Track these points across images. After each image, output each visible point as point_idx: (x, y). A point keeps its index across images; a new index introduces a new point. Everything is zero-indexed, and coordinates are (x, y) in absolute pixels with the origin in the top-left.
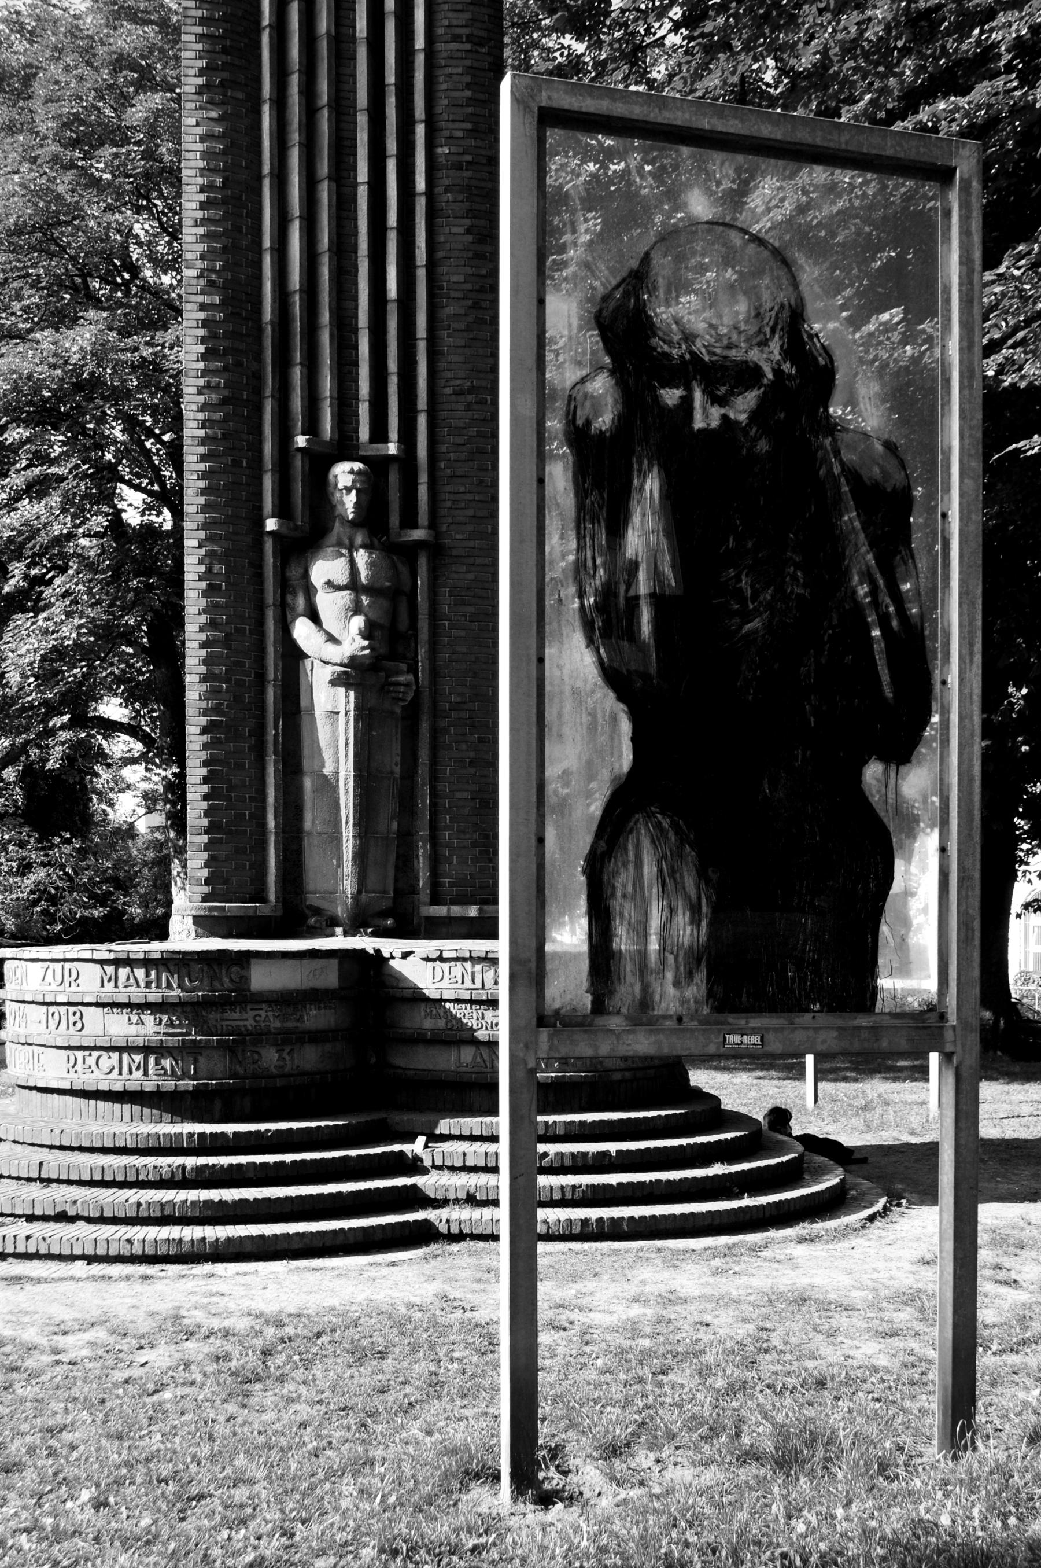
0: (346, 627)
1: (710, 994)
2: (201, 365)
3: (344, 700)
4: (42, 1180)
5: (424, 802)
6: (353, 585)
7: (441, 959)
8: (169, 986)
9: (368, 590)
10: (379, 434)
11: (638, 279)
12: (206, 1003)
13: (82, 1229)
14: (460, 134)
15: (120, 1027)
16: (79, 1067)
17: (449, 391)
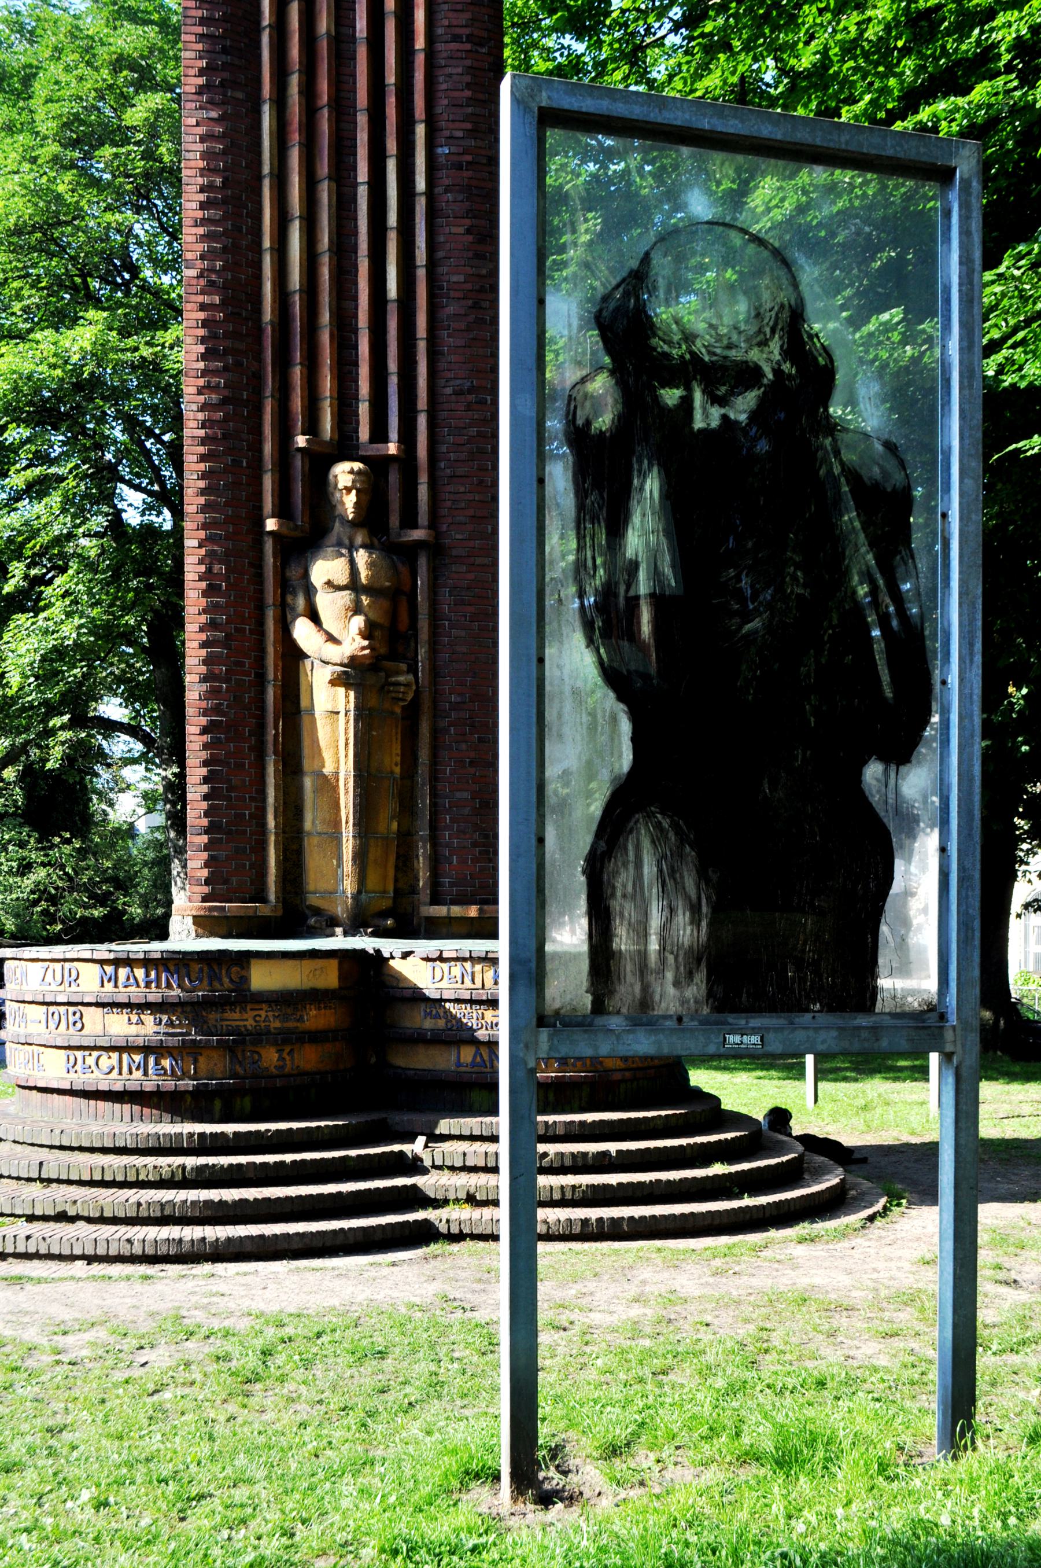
1: (710, 994)
2: (201, 365)
3: (343, 700)
4: (42, 1180)
5: (424, 803)
6: (353, 585)
7: (441, 959)
8: (169, 986)
9: (368, 590)
10: (379, 434)
11: (638, 279)
12: (207, 1003)
14: (460, 134)
15: (120, 1026)
16: (78, 1067)
17: (449, 391)
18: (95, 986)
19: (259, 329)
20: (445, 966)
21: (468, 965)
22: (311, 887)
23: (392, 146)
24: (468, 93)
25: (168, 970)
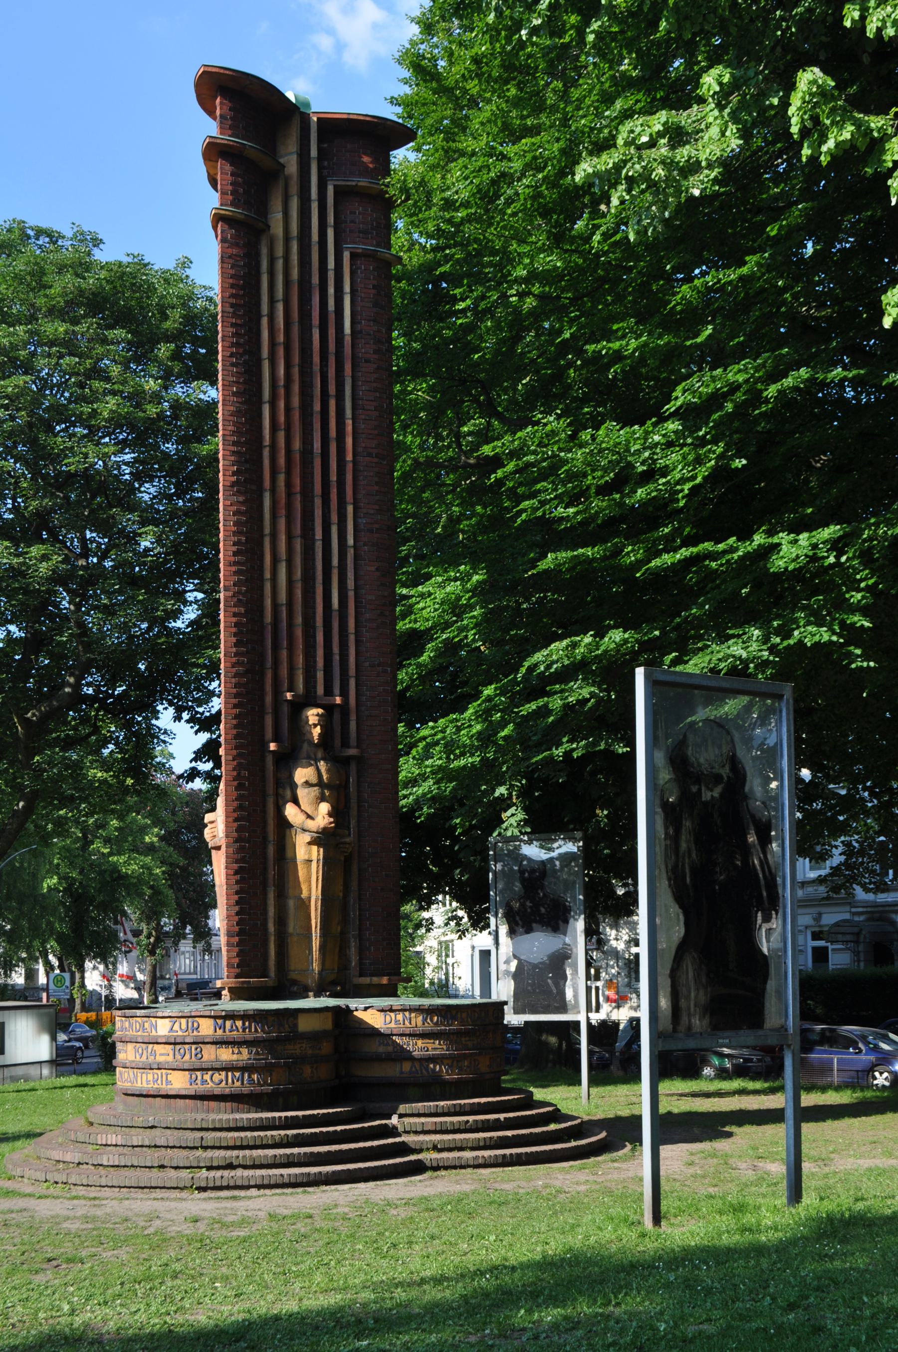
0: (317, 809)
1: (711, 1023)
2: (234, 649)
3: (316, 853)
4: (202, 1147)
5: (354, 914)
6: (320, 784)
7: (391, 1010)
8: (256, 1030)
9: (328, 786)
10: (329, 692)
11: (682, 743)
12: (278, 1040)
13: (239, 1172)
14: (372, 512)
15: (226, 1055)
16: (199, 1081)
17: (367, 664)
18: (211, 1032)
19: (262, 627)
20: (393, 1015)
21: (407, 1014)
22: (292, 968)
23: (334, 518)
24: (376, 488)
25: (255, 1021)
